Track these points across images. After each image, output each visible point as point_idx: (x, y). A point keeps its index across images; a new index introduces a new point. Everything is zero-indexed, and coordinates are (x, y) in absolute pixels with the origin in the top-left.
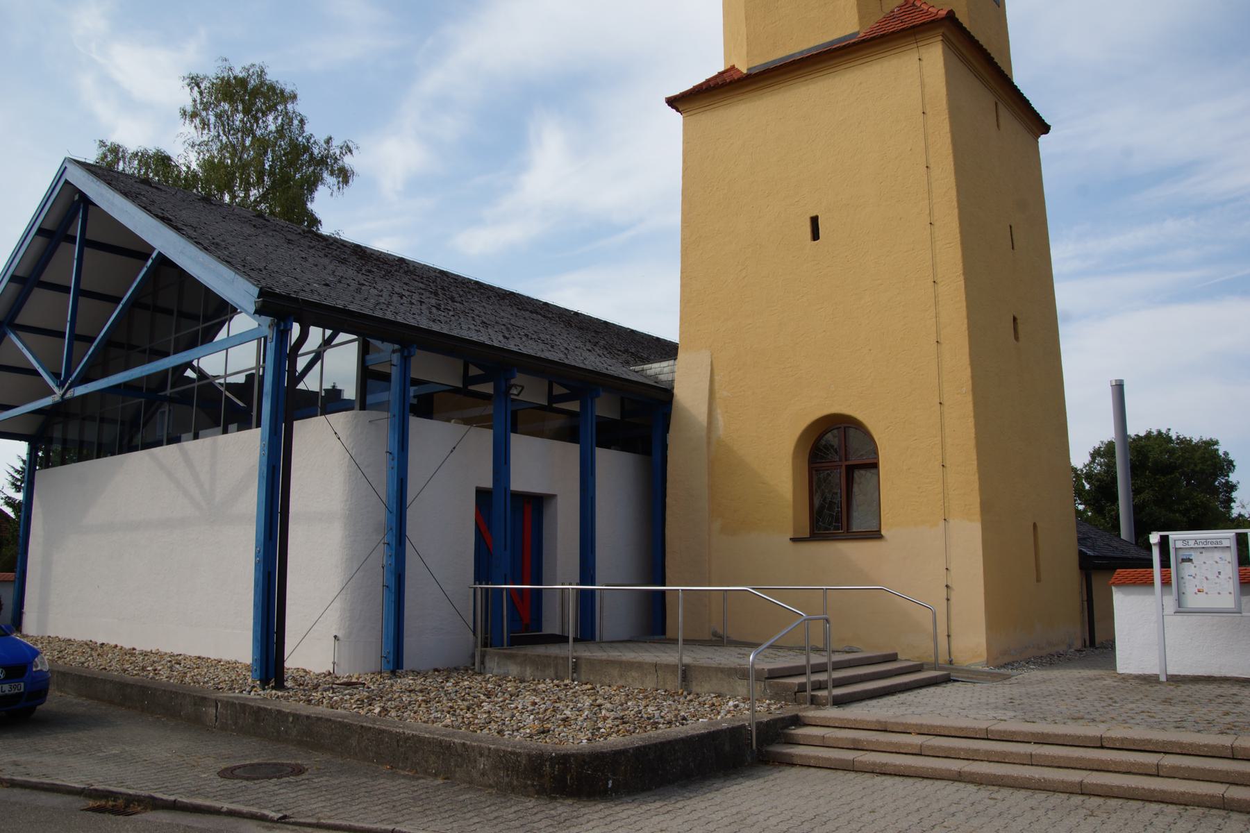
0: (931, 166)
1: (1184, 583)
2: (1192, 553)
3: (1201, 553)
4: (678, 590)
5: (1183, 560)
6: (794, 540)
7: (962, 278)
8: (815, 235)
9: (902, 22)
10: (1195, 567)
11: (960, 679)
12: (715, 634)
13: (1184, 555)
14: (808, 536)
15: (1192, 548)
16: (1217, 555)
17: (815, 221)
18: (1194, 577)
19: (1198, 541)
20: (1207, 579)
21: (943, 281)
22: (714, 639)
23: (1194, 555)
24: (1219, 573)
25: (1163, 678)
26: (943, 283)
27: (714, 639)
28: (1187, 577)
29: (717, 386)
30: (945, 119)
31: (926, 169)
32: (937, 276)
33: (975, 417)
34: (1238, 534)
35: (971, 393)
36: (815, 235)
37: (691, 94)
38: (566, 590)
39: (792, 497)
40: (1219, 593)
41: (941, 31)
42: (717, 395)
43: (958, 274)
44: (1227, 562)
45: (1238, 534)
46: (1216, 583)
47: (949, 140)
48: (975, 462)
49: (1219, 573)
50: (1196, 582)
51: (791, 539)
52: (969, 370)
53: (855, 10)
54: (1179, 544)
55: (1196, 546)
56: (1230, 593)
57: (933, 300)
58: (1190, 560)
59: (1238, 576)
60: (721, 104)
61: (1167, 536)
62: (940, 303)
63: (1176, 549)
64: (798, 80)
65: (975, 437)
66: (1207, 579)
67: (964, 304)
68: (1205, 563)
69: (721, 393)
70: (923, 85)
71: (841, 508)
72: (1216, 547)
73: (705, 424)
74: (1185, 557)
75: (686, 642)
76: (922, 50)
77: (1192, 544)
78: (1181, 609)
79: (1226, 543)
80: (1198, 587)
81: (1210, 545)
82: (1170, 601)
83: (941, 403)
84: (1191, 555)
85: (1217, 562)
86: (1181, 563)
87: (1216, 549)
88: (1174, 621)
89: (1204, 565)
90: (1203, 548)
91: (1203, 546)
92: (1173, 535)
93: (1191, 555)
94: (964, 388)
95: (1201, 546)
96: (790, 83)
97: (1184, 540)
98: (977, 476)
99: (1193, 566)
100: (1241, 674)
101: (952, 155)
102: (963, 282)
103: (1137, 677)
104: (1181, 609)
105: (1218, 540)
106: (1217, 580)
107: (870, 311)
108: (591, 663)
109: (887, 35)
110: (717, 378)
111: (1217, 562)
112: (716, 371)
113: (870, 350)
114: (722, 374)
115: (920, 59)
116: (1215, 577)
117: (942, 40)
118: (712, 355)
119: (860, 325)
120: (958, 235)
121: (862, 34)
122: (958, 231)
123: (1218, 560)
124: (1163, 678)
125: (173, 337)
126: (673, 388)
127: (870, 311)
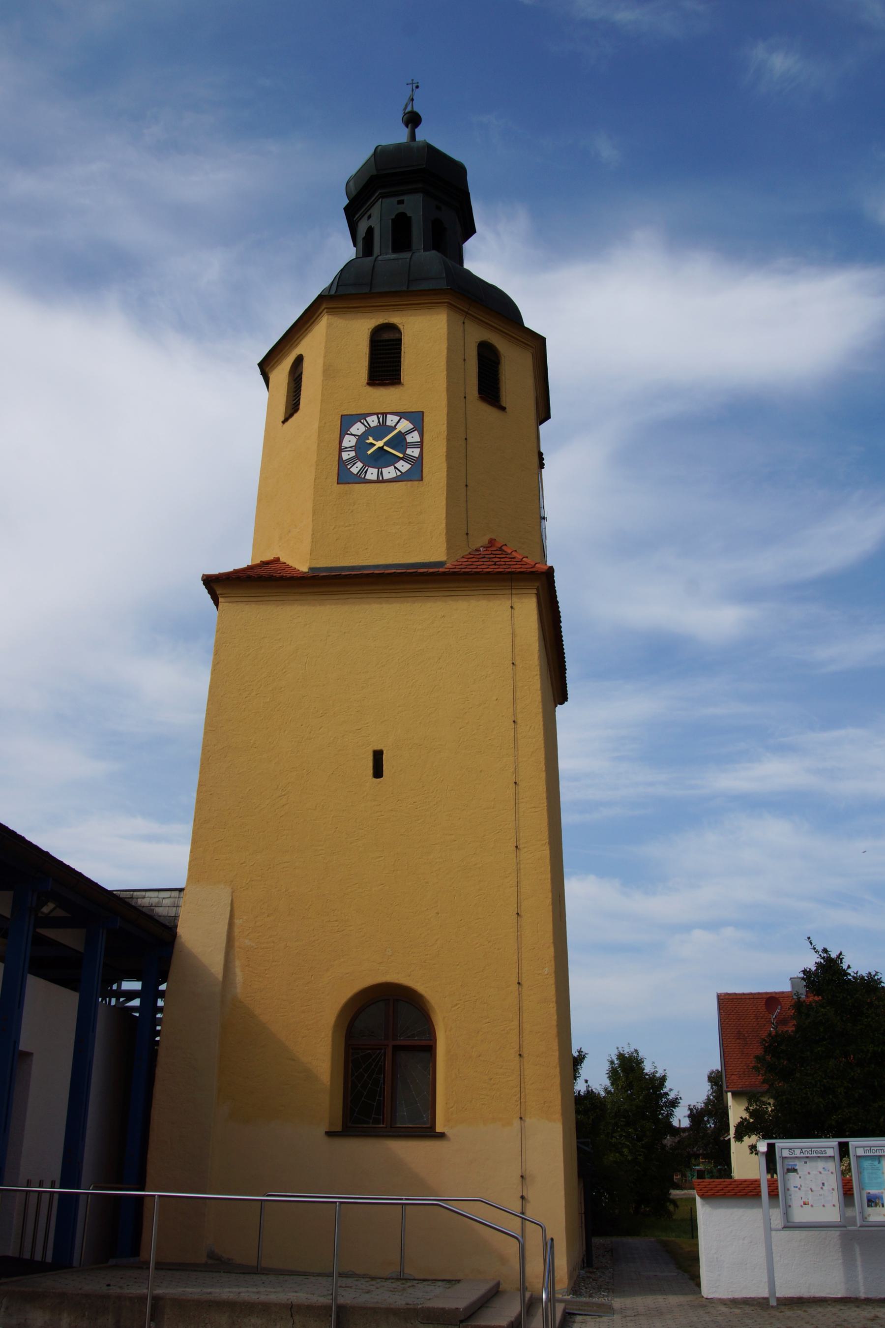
0: (519, 721)
1: (790, 1195)
2: (797, 1162)
3: (806, 1163)
4: (155, 1195)
5: (789, 1171)
6: (329, 1134)
7: (547, 847)
8: (378, 772)
9: (495, 565)
10: (800, 1177)
11: (576, 1312)
12: (211, 1255)
13: (789, 1165)
14: (341, 1130)
15: (796, 1157)
16: (821, 1165)
17: (378, 756)
18: (799, 1189)
19: (804, 1150)
20: (812, 1190)
21: (525, 847)
22: (210, 1262)
23: (799, 1165)
24: (823, 1184)
25: (773, 1303)
26: (526, 850)
27: (210, 1262)
28: (792, 1189)
29: (236, 931)
30: (536, 675)
31: (513, 723)
32: (519, 840)
33: (557, 1002)
34: (840, 1143)
35: (553, 975)
36: (378, 772)
37: (228, 578)
38: (32, 1194)
39: (329, 1079)
40: (824, 1206)
41: (537, 584)
42: (237, 944)
43: (544, 842)
44: (830, 1172)
45: (840, 1143)
46: (821, 1195)
47: (540, 698)
48: (557, 1054)
49: (823, 1184)
50: (801, 1193)
51: (326, 1133)
52: (552, 950)
53: (443, 539)
54: (786, 1153)
55: (802, 1155)
56: (834, 1205)
57: (515, 867)
58: (795, 1170)
59: (842, 1191)
60: (274, 598)
61: (847, 1144)
62: (522, 871)
63: (784, 1158)
64: (370, 595)
65: (557, 1025)
66: (812, 1190)
67: (549, 876)
68: (809, 1173)
69: (242, 941)
70: (513, 635)
71: (384, 1098)
72: (819, 1157)
73: (220, 977)
74: (790, 1168)
75: (160, 1266)
76: (515, 599)
77: (797, 1153)
78: (865, 1223)
79: (830, 1152)
80: (803, 1200)
81: (815, 1155)
82: (776, 1216)
83: (519, 983)
84: (796, 1165)
85: (820, 1173)
86: (786, 1173)
87: (819, 1159)
88: (780, 1237)
89: (808, 1175)
90: (807, 1157)
91: (809, 1155)
92: (780, 1144)
93: (796, 1165)
94: (546, 969)
95: (807, 1155)
96: (361, 596)
97: (790, 1149)
98: (558, 1070)
99: (798, 1176)
100: (829, 1294)
101: (541, 714)
102: (548, 852)
103: (734, 1302)
104: (789, 1226)
105: (823, 1150)
106: (822, 1192)
107: (440, 869)
108: (181, 1305)
109: (492, 574)
110: (237, 922)
111: (820, 1173)
112: (237, 913)
113: (438, 913)
114: (245, 917)
115: (512, 607)
116: (820, 1189)
117: (536, 594)
118: (233, 892)
119: (427, 883)
120: (545, 801)
121: (448, 565)
122: (544, 795)
123: (821, 1170)
124: (773, 1303)
125: (380, 444)
126: (176, 927)
127: (440, 869)
